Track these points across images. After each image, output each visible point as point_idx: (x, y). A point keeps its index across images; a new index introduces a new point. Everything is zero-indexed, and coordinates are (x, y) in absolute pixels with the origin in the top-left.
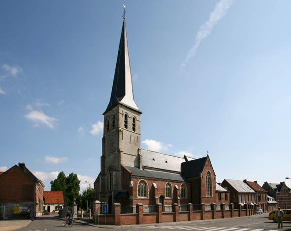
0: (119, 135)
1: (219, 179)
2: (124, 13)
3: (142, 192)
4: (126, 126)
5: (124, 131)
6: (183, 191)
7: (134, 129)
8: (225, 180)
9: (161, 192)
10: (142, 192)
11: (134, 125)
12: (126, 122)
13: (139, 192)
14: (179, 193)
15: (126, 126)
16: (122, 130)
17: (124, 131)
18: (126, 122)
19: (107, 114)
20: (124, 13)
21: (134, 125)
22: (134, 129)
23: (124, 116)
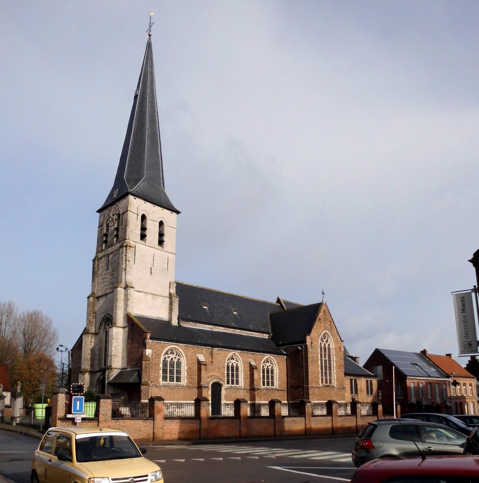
0: (178, 419)
1: (445, 355)
2: (150, 26)
3: (172, 372)
4: (143, 237)
5: (138, 245)
6: (431, 450)
7: (161, 242)
8: (469, 361)
9: (215, 374)
10: (172, 372)
11: (161, 235)
12: (143, 229)
13: (165, 371)
14: (430, 449)
15: (143, 237)
16: (132, 244)
17: (138, 245)
18: (143, 229)
19: (106, 212)
20: (150, 26)
21: (161, 235)
22: (161, 242)
23: (140, 217)
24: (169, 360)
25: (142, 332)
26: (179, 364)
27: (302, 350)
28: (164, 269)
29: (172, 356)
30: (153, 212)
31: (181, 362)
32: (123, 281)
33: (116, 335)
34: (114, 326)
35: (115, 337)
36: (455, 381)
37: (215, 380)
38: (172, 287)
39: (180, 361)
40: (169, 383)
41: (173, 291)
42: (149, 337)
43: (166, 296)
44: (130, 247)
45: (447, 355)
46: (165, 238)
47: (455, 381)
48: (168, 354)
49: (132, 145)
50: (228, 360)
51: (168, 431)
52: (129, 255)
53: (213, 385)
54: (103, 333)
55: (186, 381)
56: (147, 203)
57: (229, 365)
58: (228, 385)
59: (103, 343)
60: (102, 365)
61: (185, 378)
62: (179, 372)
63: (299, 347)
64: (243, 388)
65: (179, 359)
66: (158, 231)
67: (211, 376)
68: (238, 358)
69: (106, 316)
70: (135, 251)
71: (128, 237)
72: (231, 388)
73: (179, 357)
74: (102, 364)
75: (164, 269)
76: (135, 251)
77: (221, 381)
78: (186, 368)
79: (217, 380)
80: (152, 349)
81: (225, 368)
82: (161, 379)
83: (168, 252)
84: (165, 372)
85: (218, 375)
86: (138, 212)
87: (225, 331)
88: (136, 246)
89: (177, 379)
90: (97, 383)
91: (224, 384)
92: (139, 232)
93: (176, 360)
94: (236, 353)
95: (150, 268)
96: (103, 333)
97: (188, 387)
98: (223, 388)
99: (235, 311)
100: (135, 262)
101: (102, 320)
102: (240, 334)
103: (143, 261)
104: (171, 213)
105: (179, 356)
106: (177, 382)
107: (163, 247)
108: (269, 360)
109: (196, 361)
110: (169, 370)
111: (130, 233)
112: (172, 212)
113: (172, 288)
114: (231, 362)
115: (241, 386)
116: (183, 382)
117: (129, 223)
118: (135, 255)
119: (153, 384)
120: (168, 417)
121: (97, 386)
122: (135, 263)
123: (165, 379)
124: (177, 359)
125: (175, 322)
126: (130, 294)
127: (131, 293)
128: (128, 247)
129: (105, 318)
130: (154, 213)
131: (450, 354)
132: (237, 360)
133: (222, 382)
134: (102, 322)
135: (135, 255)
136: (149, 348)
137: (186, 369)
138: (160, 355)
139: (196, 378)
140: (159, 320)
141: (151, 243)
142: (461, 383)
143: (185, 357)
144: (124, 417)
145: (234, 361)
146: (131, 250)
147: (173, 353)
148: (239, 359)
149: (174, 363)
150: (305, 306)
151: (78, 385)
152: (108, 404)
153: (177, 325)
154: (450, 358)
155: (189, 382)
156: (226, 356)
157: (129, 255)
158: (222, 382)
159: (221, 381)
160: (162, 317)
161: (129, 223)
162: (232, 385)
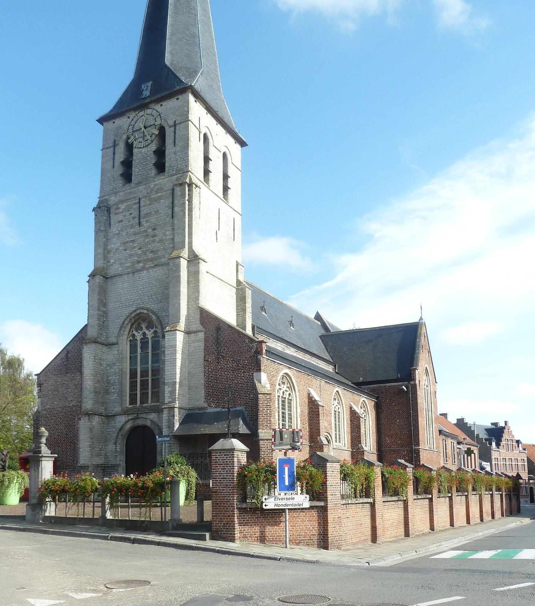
25: (247, 341)
27: (407, 392)
34: (177, 328)
36: (469, 449)
45: (441, 415)
47: (469, 449)
54: (127, 344)
59: (126, 362)
60: (126, 404)
62: (335, 414)
63: (403, 387)
64: (347, 448)
69: (138, 312)
74: (126, 401)
87: (295, 354)
90: (117, 436)
96: (127, 344)
101: (125, 319)
120: (115, 508)
121: (119, 441)
129: (133, 315)
131: (447, 414)
134: (126, 323)
144: (514, 483)
150: (342, 331)
154: (445, 419)
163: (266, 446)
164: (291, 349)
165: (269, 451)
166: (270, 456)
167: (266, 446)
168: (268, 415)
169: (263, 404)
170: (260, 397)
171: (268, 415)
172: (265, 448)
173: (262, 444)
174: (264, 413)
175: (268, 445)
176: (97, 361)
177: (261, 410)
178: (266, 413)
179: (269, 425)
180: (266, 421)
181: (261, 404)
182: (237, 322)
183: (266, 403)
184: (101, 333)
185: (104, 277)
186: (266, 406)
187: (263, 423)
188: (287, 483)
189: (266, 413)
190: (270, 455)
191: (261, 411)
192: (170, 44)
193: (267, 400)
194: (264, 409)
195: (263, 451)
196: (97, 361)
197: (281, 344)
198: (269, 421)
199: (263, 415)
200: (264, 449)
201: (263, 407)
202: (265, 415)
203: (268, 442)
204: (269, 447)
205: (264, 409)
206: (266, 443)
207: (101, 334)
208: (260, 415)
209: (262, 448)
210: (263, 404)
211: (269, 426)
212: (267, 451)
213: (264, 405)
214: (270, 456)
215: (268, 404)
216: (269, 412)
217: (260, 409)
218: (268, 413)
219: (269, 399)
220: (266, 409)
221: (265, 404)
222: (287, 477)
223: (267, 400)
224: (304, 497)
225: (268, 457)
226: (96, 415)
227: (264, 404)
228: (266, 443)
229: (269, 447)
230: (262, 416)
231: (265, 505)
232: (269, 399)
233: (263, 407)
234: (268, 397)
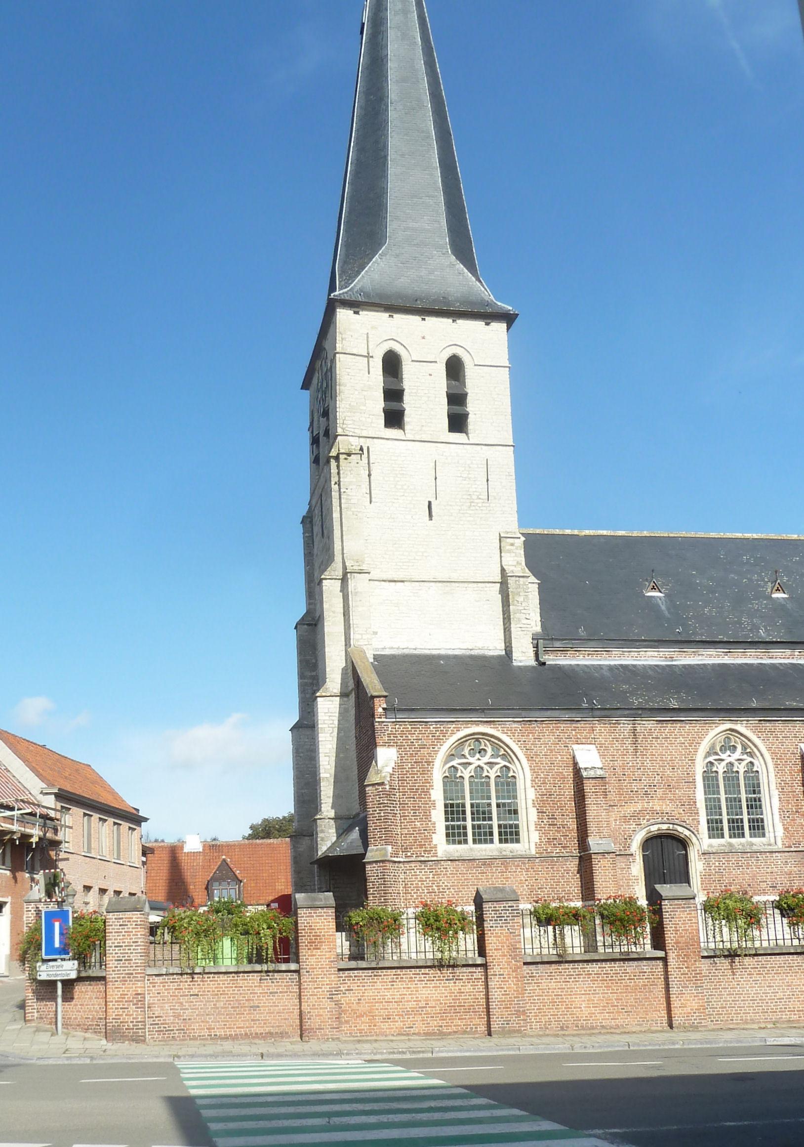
17: (376, 447)
24: (721, 768)
26: (507, 784)
28: (474, 497)
29: (475, 761)
30: (427, 337)
31: (514, 777)
32: (338, 558)
33: (327, 718)
35: (326, 726)
37: (654, 828)
38: (508, 547)
39: (511, 774)
40: (471, 849)
41: (515, 561)
42: (380, 710)
43: (497, 581)
44: (349, 455)
46: (472, 407)
48: (464, 756)
49: (353, 168)
50: (708, 754)
51: (362, 1009)
52: (345, 480)
53: (647, 844)
55: (535, 836)
56: (398, 317)
57: (737, 772)
58: (716, 842)
61: (532, 827)
62: (755, 805)
64: (780, 846)
65: (505, 766)
66: (446, 390)
67: (636, 816)
68: (749, 743)
70: (369, 463)
71: (343, 429)
72: (731, 851)
73: (504, 763)
75: (474, 497)
76: (369, 463)
77: (680, 829)
78: (532, 794)
79: (665, 827)
80: (400, 747)
81: (694, 782)
82: (439, 837)
83: (486, 445)
84: (756, 808)
85: (667, 807)
86: (370, 347)
88: (371, 450)
89: (713, 830)
91: (694, 839)
92: (441, 410)
93: (741, 768)
94: (739, 727)
95: (427, 504)
97: (544, 857)
98: (693, 855)
99: (778, 590)
100: (373, 496)
102: (794, 661)
103: (399, 487)
104: (423, 319)
105: (504, 757)
106: (506, 841)
107: (467, 434)
108: (735, 740)
109: (571, 769)
110: (727, 801)
111: (349, 414)
112: (454, 319)
113: (509, 551)
114: (722, 760)
115: (772, 841)
116: (526, 840)
117: (342, 388)
118: (369, 475)
119: (409, 854)
122: (373, 500)
123: (455, 834)
124: (744, 763)
125: (524, 656)
126: (357, 593)
127: (359, 590)
128: (342, 457)
130: (423, 338)
132: (748, 750)
133: (687, 833)
135: (369, 475)
136: (388, 744)
137: (534, 797)
138: (428, 763)
139: (572, 824)
140: (473, 658)
141: (424, 428)
142: (465, 777)
143: (767, 756)
145: (737, 754)
146: (353, 464)
147: (482, 751)
148: (753, 747)
149: (488, 784)
151: (44, 870)
152: (130, 927)
153: (532, 662)
155: (549, 841)
156: (695, 743)
157: (345, 480)
158: (687, 833)
159: (680, 829)
160: (480, 645)
161: (342, 388)
162: (734, 841)
163: (375, 873)
164: (704, 653)
165: (380, 880)
166: (381, 890)
167: (375, 873)
168: (381, 819)
169: (374, 802)
170: (369, 790)
171: (381, 819)
172: (374, 876)
173: (370, 870)
174: (376, 817)
175: (379, 871)
176: (302, 755)
177: (371, 812)
178: (379, 817)
179: (384, 836)
180: (379, 830)
181: (371, 802)
182: (505, 643)
183: (378, 799)
184: (309, 711)
185: (309, 625)
186: (378, 804)
187: (375, 835)
188: (57, 944)
189: (379, 817)
190: (383, 888)
191: (371, 814)
192: (435, 183)
193: (378, 795)
194: (376, 811)
195: (371, 882)
196: (302, 755)
197: (658, 651)
198: (383, 830)
199: (374, 820)
200: (373, 878)
201: (374, 807)
202: (377, 820)
203: (378, 867)
204: (379, 874)
205: (376, 811)
206: (375, 867)
207: (309, 712)
208: (370, 820)
209: (369, 876)
210: (374, 802)
211: (383, 838)
212: (377, 882)
213: (375, 804)
214: (381, 890)
215: (381, 802)
216: (382, 815)
217: (370, 811)
218: (381, 816)
219: (381, 791)
220: (379, 810)
221: (377, 801)
222: (58, 935)
223: (378, 795)
224: (72, 965)
225: (379, 891)
226: (304, 836)
227: (375, 802)
228: (375, 867)
229: (379, 874)
230: (373, 823)
231: (40, 975)
232: (381, 791)
233: (374, 807)
234: (381, 790)
